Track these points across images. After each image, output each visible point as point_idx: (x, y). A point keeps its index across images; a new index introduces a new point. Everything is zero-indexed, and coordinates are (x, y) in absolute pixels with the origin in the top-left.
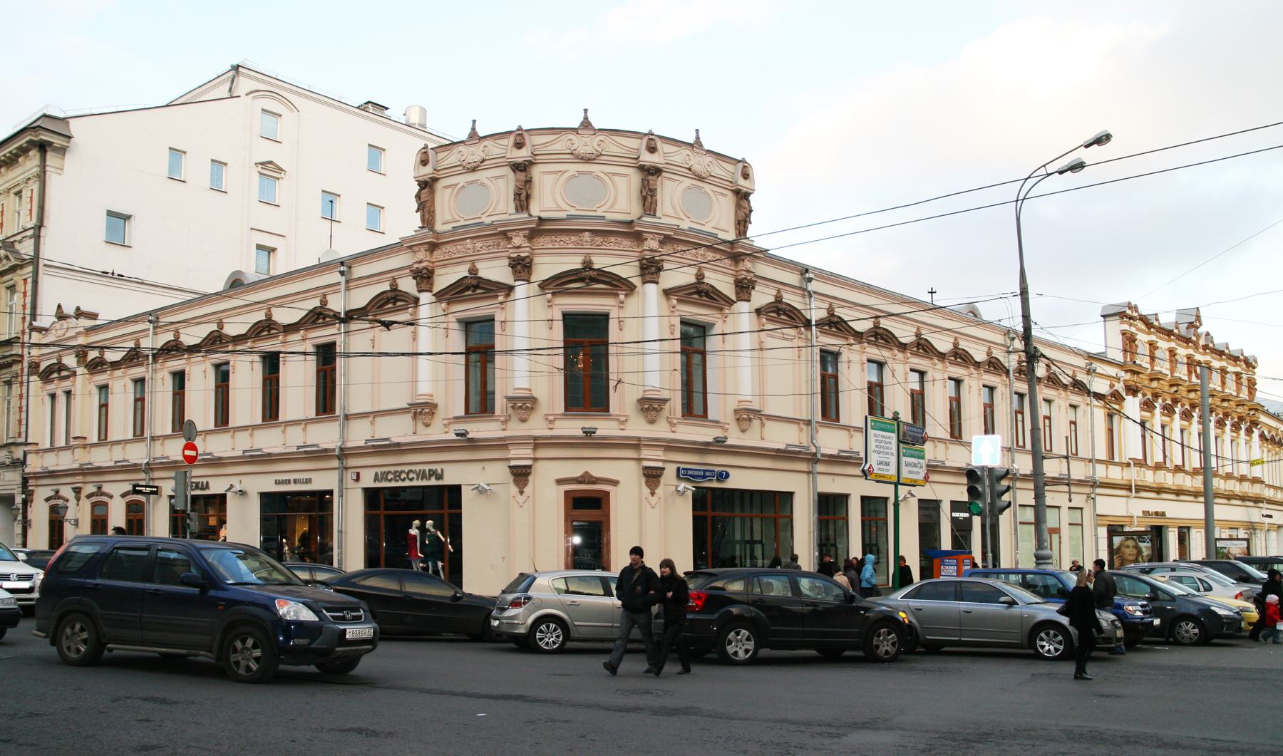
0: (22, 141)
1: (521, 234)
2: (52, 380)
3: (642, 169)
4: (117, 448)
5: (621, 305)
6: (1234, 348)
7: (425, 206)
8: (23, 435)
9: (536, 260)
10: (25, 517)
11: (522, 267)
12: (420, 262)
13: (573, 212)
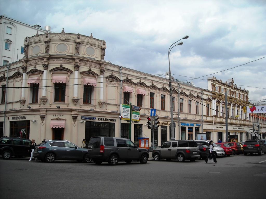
1: (46, 58)
6: (242, 89)
11: (46, 67)
12: (24, 65)
13: (59, 53)
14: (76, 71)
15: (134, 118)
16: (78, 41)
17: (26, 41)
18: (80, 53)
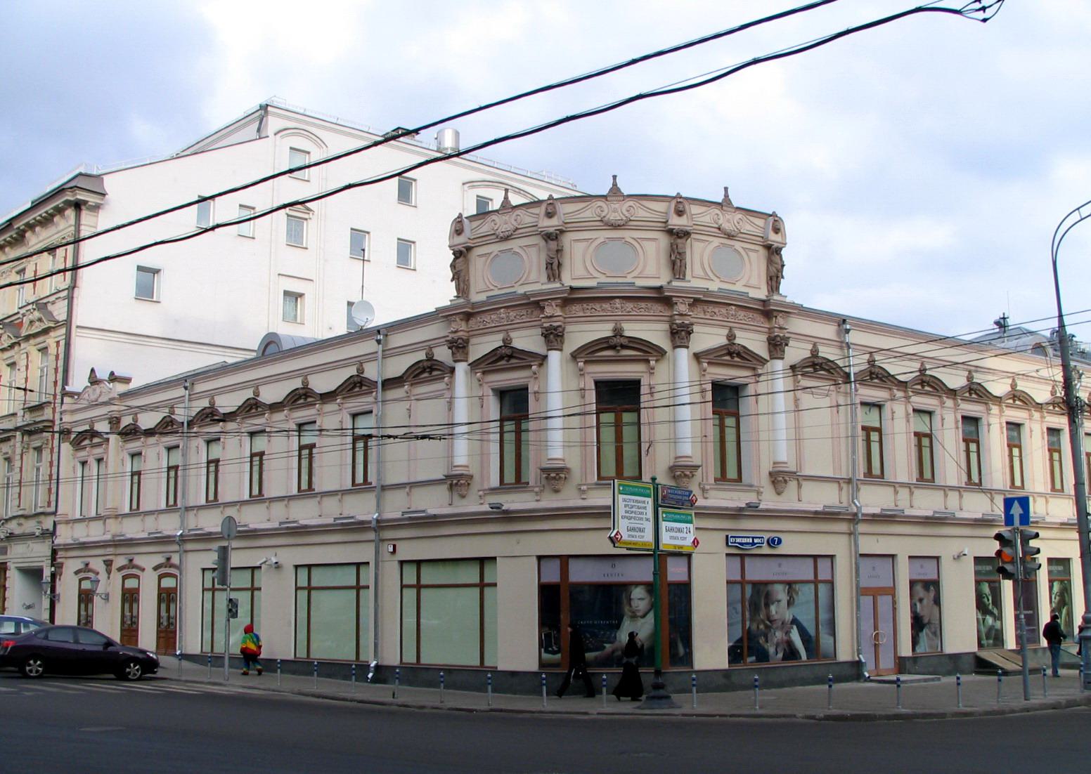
0: (59, 202)
2: (84, 448)
3: (670, 232)
4: (150, 520)
5: (651, 371)
7: (460, 276)
8: (53, 504)
9: (569, 328)
10: (53, 589)
11: (554, 337)
12: (456, 332)
14: (678, 349)
15: (671, 538)
16: (677, 228)
17: (457, 231)
18: (688, 277)
